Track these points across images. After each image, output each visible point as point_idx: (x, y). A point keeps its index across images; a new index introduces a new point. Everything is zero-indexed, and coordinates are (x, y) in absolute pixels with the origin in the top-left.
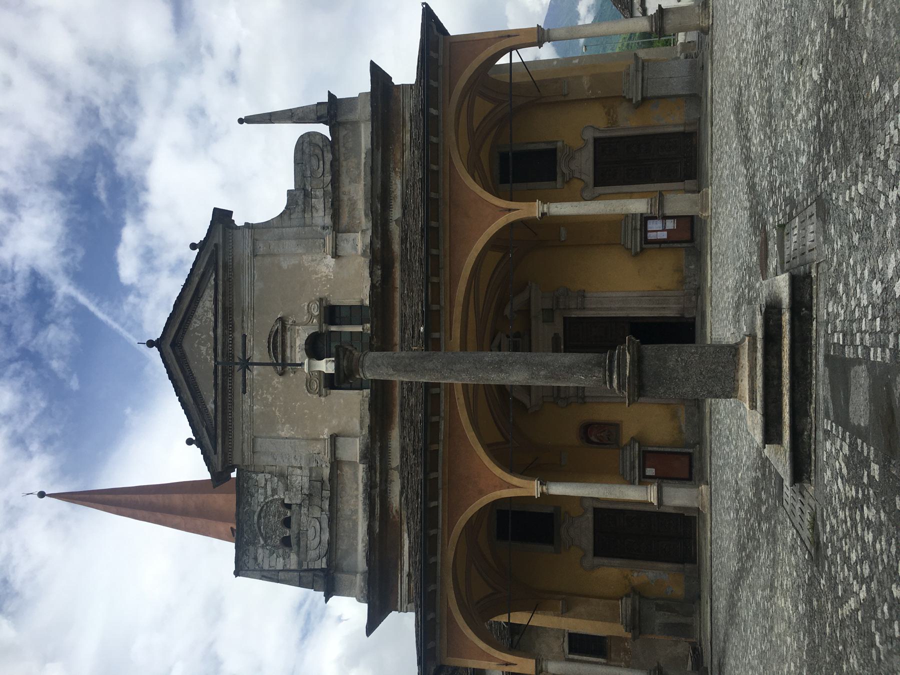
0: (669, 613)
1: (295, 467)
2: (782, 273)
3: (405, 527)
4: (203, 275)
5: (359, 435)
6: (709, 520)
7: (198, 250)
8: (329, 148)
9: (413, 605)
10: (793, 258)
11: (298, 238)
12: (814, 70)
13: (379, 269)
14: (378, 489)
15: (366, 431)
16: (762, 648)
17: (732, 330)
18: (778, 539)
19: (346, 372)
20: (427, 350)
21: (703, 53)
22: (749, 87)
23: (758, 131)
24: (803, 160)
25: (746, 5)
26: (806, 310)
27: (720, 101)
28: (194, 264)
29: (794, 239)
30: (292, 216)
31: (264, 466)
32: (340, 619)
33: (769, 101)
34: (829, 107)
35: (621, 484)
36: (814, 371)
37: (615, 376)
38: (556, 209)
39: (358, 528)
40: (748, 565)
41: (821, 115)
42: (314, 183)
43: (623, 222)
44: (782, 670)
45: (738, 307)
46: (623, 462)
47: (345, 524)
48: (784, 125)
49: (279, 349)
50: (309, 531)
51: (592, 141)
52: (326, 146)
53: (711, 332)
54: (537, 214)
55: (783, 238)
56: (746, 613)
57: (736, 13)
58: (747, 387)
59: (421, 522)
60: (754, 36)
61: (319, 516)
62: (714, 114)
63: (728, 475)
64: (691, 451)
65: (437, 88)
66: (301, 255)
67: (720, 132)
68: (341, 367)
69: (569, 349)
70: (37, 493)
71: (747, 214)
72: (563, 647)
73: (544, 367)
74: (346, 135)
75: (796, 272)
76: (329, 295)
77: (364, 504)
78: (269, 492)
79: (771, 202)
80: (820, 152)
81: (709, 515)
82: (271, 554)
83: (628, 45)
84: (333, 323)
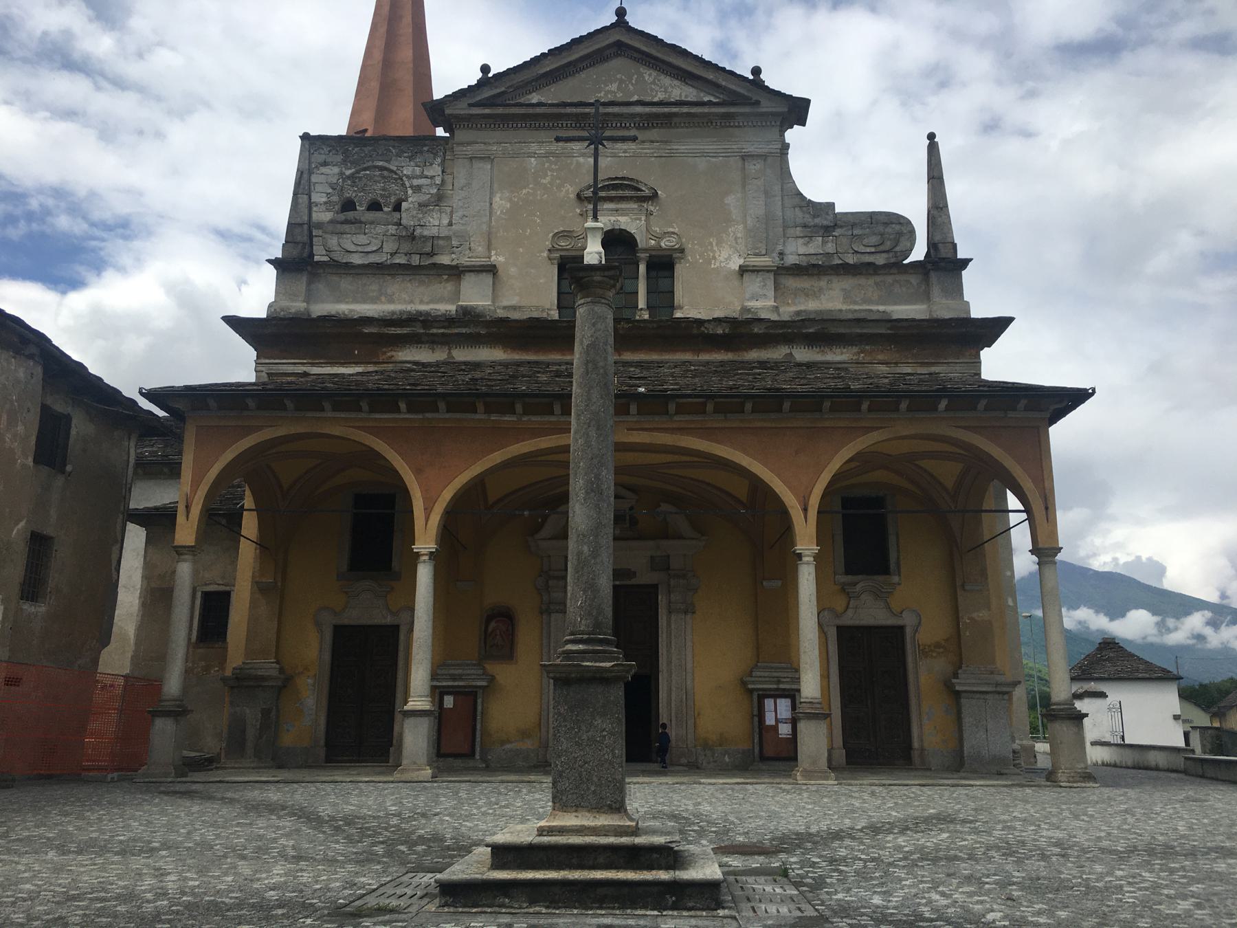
0: (258, 727)
2: (723, 873)
3: (371, 368)
4: (717, 86)
5: (497, 305)
6: (385, 779)
7: (751, 77)
8: (893, 260)
9: (265, 378)
10: (742, 887)
12: (999, 915)
13: (724, 330)
14: (422, 331)
15: (501, 314)
16: (216, 845)
17: (642, 810)
18: (363, 866)
20: (617, 396)
21: (1019, 774)
22: (974, 833)
23: (914, 844)
24: (877, 900)
25: (1087, 830)
27: (955, 795)
28: (732, 73)
29: (769, 889)
30: (797, 209)
31: (452, 173)
32: (242, 282)
33: (956, 858)
35: (432, 663)
36: (590, 912)
37: (581, 647)
38: (806, 574)
39: (369, 303)
40: (326, 829)
41: (938, 923)
42: (844, 240)
43: (789, 665)
44: (189, 871)
45: (673, 817)
47: (373, 286)
48: (923, 876)
49: (613, 193)
51: (900, 622)
52: (896, 257)
53: (638, 783)
54: (799, 548)
55: (769, 875)
56: (261, 825)
57: (1076, 817)
58: (568, 824)
59: (379, 389)
60: (1044, 840)
62: (937, 788)
63: (446, 803)
64: (477, 757)
65: (975, 409)
67: (912, 795)
68: (593, 274)
69: (618, 592)
71: (802, 829)
72: (211, 584)
73: (593, 552)
75: (724, 890)
77: (402, 312)
78: (416, 182)
79: (818, 860)
80: (888, 921)
81: (391, 779)
83: (1031, 676)
84: (649, 268)
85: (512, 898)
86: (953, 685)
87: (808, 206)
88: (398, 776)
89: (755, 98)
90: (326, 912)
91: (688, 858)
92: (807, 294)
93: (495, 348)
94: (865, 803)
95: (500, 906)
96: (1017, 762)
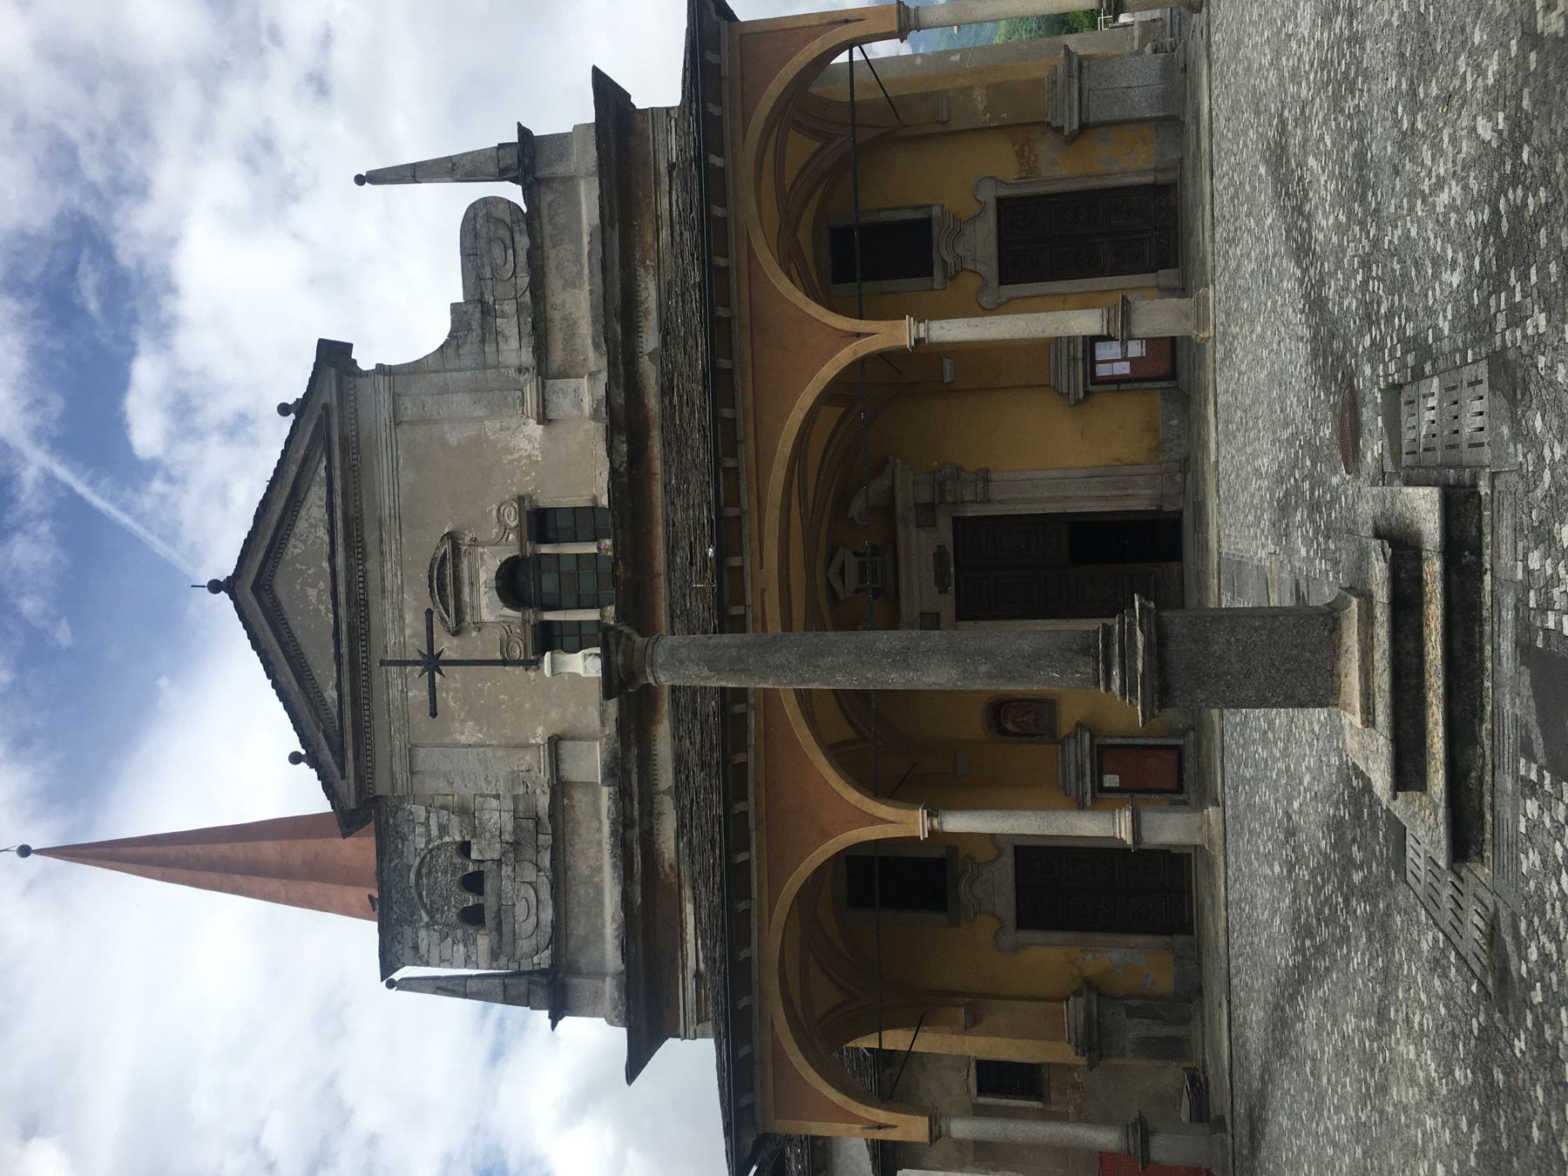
1: (488, 795)
3: (687, 893)
4: (305, 460)
5: (599, 734)
6: (1222, 866)
8: (523, 226)
9: (709, 1026)
11: (475, 389)
13: (623, 443)
14: (637, 829)
15: (611, 729)
17: (1271, 548)
19: (622, 675)
21: (1185, 45)
24: (1455, 279)
26: (1471, 554)
27: (1230, 135)
31: (432, 797)
33: (1360, 156)
34: (1525, 197)
37: (1116, 672)
38: (941, 332)
42: (500, 289)
46: (1064, 767)
47: (581, 892)
49: (450, 590)
50: (517, 906)
51: (992, 204)
53: (1219, 542)
54: (908, 342)
59: (721, 888)
61: (533, 878)
62: (1216, 156)
63: (1264, 796)
64: (1180, 742)
66: (481, 419)
68: (613, 666)
70: (16, 849)
71: (1304, 350)
72: (967, 1086)
73: (986, 659)
74: (553, 202)
76: (534, 490)
77: (613, 855)
78: (435, 832)
82: (443, 938)
85: (1469, 766)
86: (1072, 133)
87: (457, 337)
88: (1217, 848)
89: (319, 411)
90: (1497, 1015)
91: (1394, 524)
92: (571, 335)
93: (655, 735)
94: (1248, 255)
95: (1482, 783)
96: (1168, 48)
